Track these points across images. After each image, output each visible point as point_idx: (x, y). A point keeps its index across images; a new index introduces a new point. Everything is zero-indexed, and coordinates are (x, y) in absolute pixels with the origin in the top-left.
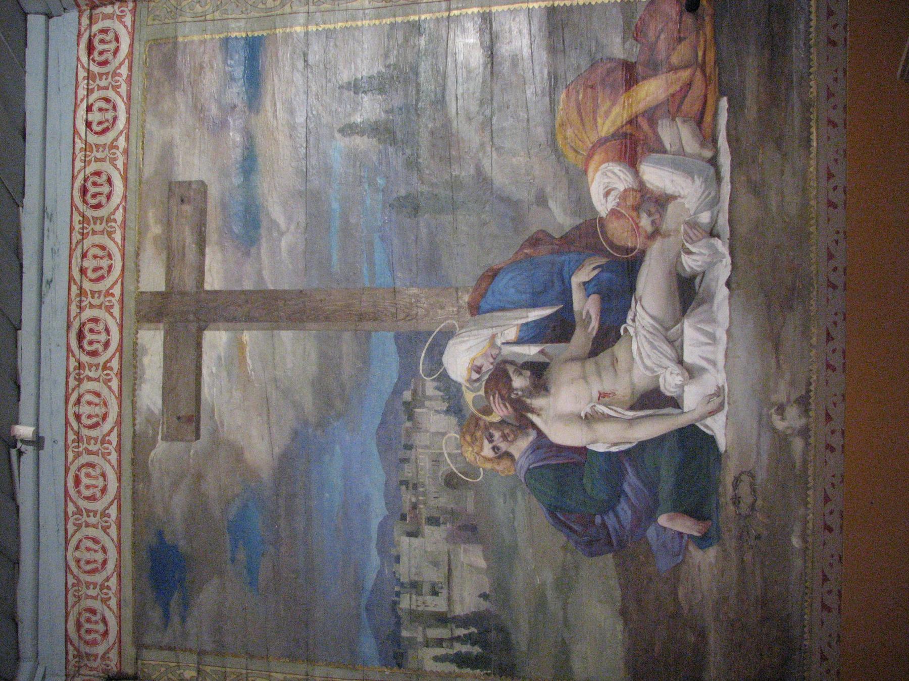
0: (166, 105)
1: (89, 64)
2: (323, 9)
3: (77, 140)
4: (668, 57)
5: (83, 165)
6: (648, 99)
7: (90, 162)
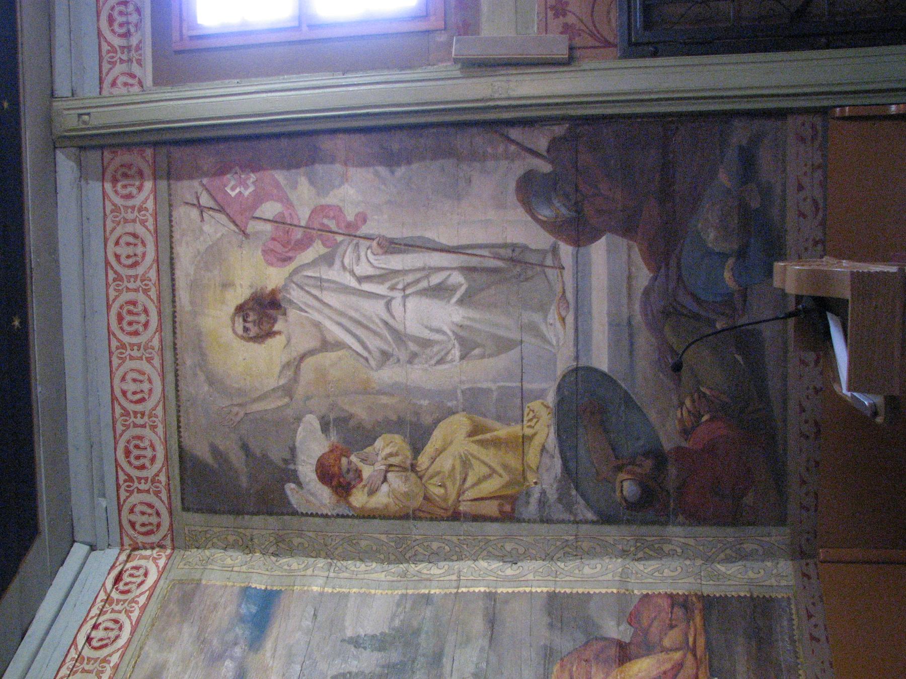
0: (172, 631)
1: (111, 591)
2: (342, 577)
3: (72, 650)
4: (661, 639)
5: (68, 672)
6: (640, 674)
7: (76, 672)
